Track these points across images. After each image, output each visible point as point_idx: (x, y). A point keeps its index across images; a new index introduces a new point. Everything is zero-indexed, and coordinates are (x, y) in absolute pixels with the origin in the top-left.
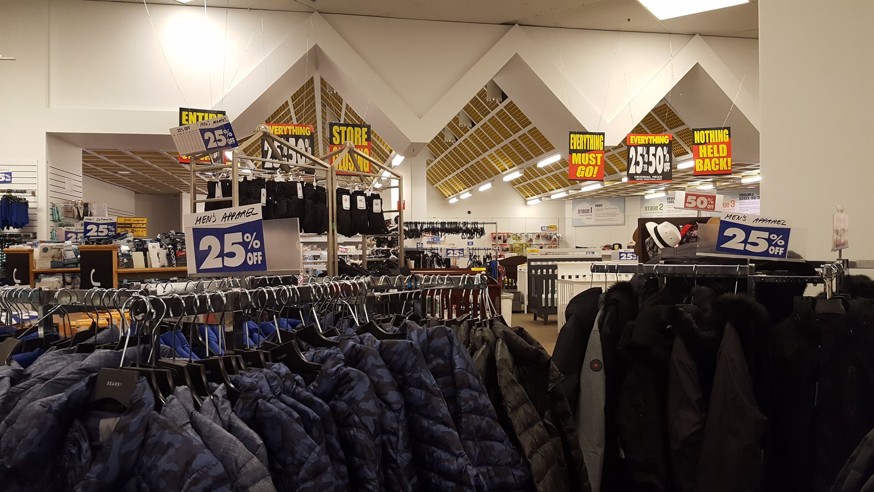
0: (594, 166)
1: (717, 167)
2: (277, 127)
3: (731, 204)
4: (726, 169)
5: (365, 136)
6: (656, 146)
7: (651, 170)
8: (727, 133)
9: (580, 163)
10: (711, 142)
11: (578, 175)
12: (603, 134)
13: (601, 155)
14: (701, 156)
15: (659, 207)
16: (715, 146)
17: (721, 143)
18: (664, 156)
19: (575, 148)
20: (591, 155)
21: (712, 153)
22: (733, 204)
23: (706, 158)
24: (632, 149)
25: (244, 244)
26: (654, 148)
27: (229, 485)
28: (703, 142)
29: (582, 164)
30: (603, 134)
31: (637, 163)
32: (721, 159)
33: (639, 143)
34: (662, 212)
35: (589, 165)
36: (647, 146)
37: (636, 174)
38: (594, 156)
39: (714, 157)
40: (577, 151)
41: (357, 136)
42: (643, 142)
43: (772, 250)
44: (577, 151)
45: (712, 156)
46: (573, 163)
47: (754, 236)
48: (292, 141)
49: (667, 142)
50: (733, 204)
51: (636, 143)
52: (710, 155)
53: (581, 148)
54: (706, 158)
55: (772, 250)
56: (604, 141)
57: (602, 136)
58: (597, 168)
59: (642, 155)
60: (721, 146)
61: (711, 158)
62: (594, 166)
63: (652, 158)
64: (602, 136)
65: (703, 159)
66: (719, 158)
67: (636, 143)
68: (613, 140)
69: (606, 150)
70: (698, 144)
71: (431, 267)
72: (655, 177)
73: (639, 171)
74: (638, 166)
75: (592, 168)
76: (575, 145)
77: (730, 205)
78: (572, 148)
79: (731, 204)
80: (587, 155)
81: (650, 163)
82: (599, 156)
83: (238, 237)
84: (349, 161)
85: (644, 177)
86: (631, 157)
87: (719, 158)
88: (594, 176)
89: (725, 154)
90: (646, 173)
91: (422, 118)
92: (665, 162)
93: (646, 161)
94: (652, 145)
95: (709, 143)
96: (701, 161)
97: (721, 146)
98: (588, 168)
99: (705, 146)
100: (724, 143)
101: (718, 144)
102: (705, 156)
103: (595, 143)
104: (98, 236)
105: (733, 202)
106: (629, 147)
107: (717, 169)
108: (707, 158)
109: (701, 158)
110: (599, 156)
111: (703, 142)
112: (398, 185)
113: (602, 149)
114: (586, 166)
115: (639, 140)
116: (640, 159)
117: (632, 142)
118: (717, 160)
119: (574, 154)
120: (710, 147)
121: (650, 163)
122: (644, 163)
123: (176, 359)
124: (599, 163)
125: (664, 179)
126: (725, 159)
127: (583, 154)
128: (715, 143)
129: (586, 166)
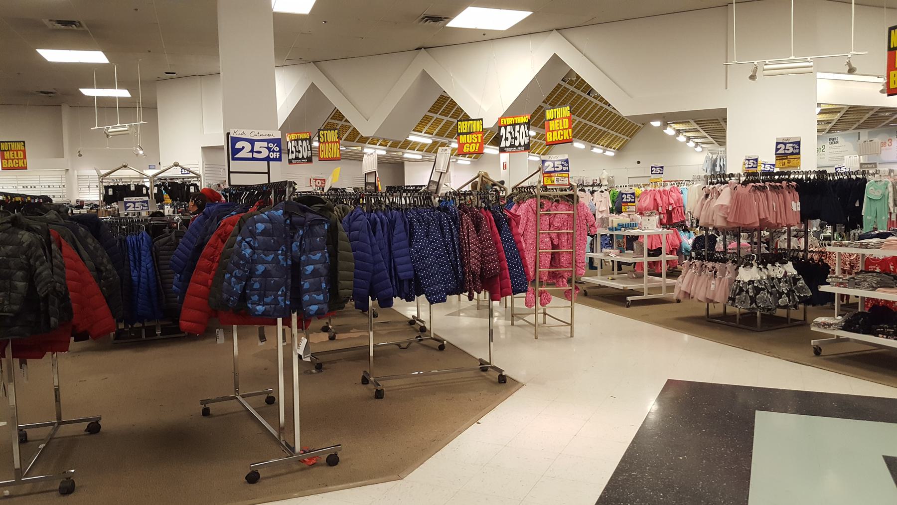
0: (476, 143)
1: (562, 137)
2: (508, 119)
3: (888, 143)
4: (568, 138)
5: (337, 136)
6: (520, 124)
7: (517, 144)
8: (569, 109)
9: (466, 142)
10: (558, 117)
11: (465, 151)
12: (482, 119)
13: (481, 135)
14: (6, 158)
15: (822, 149)
16: (15, 152)
17: (19, 150)
18: (307, 146)
19: (462, 132)
20: (473, 135)
21: (559, 126)
22: (891, 142)
23: (554, 131)
24: (503, 129)
25: (631, 197)
26: (518, 126)
27: (467, 294)
28: (552, 118)
29: (467, 143)
30: (482, 119)
31: (507, 139)
32: (565, 131)
33: (508, 123)
34: (824, 155)
35: (472, 142)
36: (514, 125)
37: (506, 147)
38: (476, 136)
39: (560, 130)
40: (463, 134)
41: (333, 136)
42: (510, 122)
43: (272, 155)
44: (463, 134)
45: (13, 158)
46: (461, 142)
47: (766, 166)
48: (300, 142)
49: (527, 121)
50: (891, 142)
51: (505, 123)
52: (12, 158)
53: (466, 131)
54: (554, 131)
55: (272, 155)
56: (482, 125)
57: (481, 121)
58: (478, 145)
59: (510, 133)
60: (564, 120)
61: (557, 131)
62: (476, 143)
63: (517, 135)
64: (481, 121)
65: (7, 160)
66: (18, 159)
67: (505, 123)
68: (489, 123)
69: (484, 131)
70: (3, 151)
71: (362, 214)
72: (519, 148)
73: (508, 145)
74: (508, 140)
75: (475, 145)
76: (461, 129)
77: (887, 145)
78: (459, 132)
79: (888, 143)
80: (471, 135)
81: (516, 138)
82: (480, 136)
83: (630, 195)
84: (329, 152)
85: (512, 149)
86: (501, 134)
87: (18, 159)
88: (476, 151)
89: (22, 157)
90: (297, 158)
91: (370, 120)
92: (308, 150)
93: (513, 137)
94: (517, 124)
95: (11, 150)
96: (6, 161)
97: (564, 120)
98: (471, 141)
99: (8, 152)
100: (21, 150)
101: (17, 151)
102: (554, 129)
103: (476, 127)
104: (135, 210)
105: (890, 141)
106: (500, 127)
107: (17, 166)
108: (555, 130)
109: (6, 159)
110: (480, 136)
111: (552, 118)
112: (267, 171)
113: (481, 130)
114: (470, 144)
115: (508, 121)
116: (508, 135)
117: (502, 123)
118: (561, 131)
119: (461, 136)
120: (11, 152)
121: (516, 138)
122: (512, 138)
123: (779, 248)
124: (480, 141)
125: (525, 150)
126: (567, 130)
127: (468, 136)
128: (15, 151)
129: (470, 144)
